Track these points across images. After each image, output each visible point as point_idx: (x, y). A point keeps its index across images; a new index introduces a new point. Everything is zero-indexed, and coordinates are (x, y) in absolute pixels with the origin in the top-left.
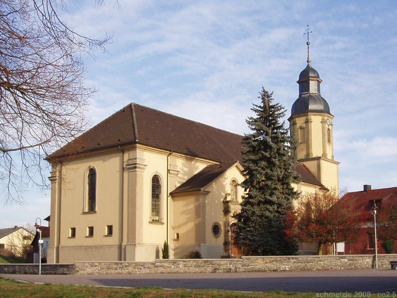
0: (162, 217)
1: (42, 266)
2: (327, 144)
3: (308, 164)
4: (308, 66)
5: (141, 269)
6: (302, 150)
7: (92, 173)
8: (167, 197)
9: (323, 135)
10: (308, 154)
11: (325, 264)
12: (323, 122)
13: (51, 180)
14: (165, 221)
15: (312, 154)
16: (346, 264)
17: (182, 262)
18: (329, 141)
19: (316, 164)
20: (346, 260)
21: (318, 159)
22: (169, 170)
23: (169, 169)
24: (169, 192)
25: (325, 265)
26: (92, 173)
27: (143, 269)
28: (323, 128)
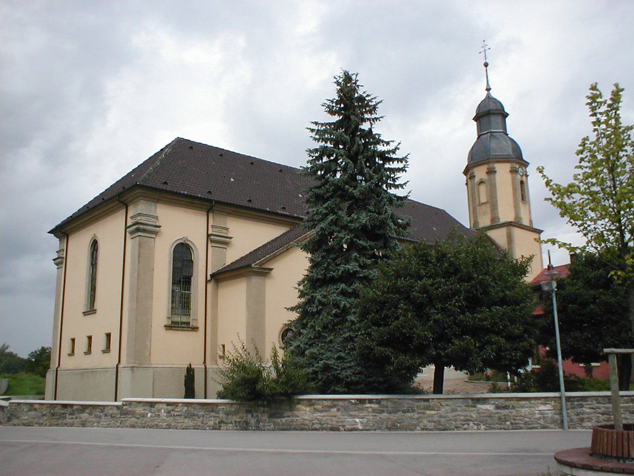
0: (86, 307)
1: (566, 390)
2: (521, 203)
3: (494, 234)
4: (489, 97)
5: (100, 417)
6: (484, 213)
7: (95, 244)
8: (207, 282)
9: (514, 189)
10: (494, 218)
11: (441, 416)
12: (514, 171)
13: (56, 264)
14: (201, 324)
15: (499, 219)
16: (490, 416)
17: (165, 406)
18: (524, 198)
19: (505, 234)
20: (489, 407)
21: (509, 224)
22: (211, 235)
23: (209, 233)
24: (209, 273)
25: (442, 420)
26: (95, 244)
27: (103, 417)
28: (513, 180)
